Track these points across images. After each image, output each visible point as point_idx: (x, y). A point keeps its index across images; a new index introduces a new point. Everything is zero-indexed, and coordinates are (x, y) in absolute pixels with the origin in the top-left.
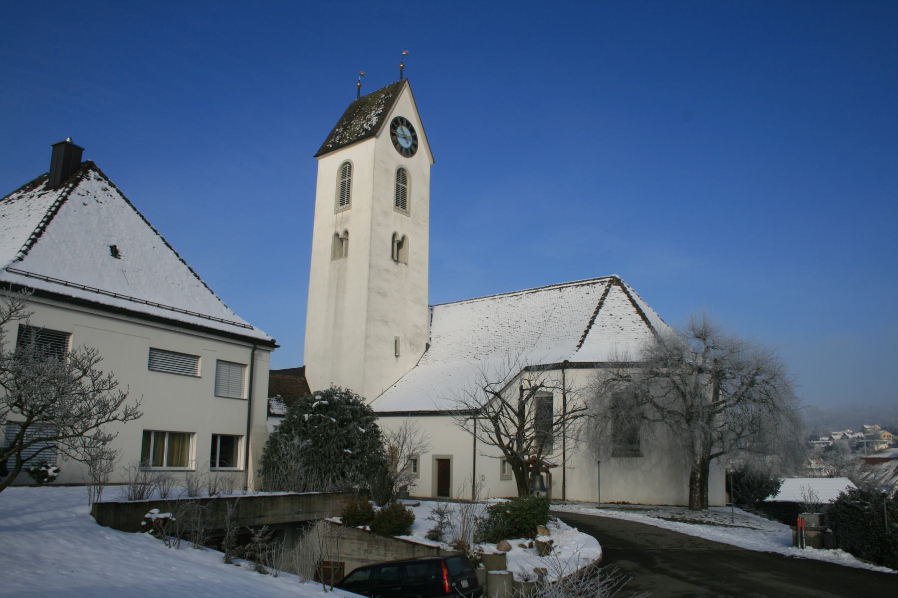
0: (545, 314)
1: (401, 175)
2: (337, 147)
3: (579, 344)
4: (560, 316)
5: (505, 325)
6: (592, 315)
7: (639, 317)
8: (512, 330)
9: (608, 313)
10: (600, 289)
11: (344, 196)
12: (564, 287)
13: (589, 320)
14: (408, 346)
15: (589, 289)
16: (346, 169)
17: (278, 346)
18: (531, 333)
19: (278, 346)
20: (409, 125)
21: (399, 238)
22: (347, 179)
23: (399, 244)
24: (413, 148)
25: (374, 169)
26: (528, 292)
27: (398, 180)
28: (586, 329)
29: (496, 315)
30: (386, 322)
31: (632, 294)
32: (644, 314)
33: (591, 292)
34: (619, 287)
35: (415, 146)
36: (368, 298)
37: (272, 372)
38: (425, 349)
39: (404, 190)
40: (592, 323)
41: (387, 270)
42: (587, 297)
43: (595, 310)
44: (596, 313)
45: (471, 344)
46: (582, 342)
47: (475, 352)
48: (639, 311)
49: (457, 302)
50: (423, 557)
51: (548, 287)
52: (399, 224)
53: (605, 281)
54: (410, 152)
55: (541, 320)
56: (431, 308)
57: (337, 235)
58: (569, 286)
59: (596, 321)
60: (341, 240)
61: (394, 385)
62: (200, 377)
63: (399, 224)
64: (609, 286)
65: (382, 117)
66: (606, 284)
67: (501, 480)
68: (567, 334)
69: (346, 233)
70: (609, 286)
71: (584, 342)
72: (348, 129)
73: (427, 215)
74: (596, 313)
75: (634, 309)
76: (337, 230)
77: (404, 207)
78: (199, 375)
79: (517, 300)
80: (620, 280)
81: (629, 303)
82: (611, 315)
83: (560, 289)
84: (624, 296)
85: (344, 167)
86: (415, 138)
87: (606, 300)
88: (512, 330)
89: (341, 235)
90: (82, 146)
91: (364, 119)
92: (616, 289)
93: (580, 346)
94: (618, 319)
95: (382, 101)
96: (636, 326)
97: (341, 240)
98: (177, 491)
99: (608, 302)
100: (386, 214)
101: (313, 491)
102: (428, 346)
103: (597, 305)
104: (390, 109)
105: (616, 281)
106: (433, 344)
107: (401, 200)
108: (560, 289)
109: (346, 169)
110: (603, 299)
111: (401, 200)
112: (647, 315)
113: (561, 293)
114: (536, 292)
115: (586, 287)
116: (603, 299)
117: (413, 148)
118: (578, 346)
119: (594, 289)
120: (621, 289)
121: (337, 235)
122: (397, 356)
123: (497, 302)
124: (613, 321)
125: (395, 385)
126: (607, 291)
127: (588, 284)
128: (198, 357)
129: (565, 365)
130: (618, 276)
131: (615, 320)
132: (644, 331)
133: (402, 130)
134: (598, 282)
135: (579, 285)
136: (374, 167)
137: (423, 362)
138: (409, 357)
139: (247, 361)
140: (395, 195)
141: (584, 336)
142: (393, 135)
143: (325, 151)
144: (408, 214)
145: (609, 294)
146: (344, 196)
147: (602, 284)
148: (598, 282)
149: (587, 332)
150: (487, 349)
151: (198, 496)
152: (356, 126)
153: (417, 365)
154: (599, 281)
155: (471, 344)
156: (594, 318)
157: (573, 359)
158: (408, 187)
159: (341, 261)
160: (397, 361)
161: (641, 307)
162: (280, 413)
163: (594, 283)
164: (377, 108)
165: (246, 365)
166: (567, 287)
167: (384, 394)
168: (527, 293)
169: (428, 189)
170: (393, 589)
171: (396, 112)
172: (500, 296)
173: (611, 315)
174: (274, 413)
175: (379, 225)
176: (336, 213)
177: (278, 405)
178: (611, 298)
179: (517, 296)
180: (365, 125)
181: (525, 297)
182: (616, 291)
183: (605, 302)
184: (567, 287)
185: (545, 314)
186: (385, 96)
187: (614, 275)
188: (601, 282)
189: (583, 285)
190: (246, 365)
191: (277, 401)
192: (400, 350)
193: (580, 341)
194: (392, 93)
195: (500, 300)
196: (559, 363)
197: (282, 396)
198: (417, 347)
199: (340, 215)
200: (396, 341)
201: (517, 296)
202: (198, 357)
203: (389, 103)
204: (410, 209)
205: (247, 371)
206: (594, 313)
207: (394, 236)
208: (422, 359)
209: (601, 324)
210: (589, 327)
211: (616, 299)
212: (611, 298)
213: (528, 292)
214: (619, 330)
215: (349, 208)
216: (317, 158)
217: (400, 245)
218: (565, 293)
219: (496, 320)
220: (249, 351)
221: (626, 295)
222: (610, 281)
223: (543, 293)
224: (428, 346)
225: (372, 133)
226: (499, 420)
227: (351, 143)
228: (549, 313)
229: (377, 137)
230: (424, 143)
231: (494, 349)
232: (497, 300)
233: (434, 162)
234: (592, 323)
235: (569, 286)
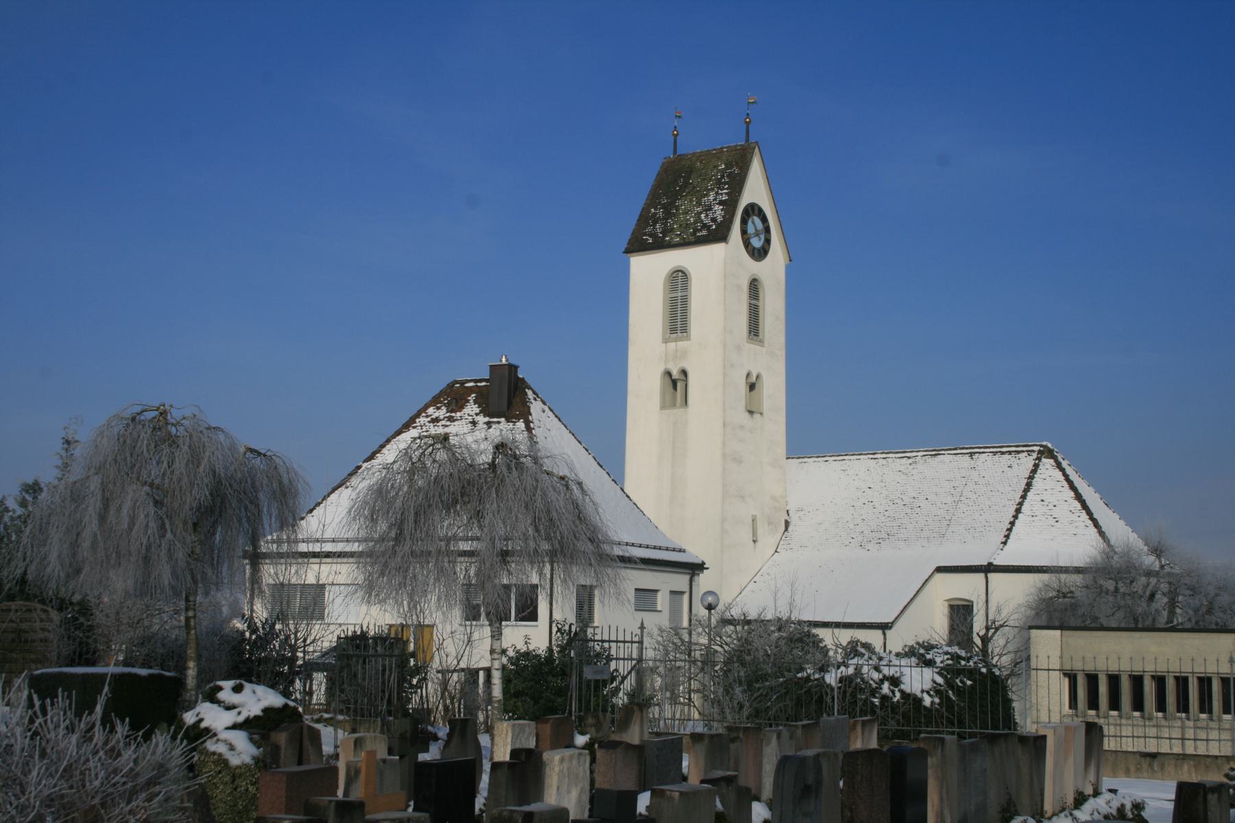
0: (953, 491)
2: (660, 245)
3: (1004, 540)
4: (974, 496)
5: (898, 501)
6: (1018, 500)
7: (1078, 505)
8: (909, 511)
9: (1039, 498)
10: (1027, 462)
12: (977, 453)
13: (1015, 507)
15: (1013, 459)
16: (679, 279)
17: (707, 568)
18: (936, 518)
19: (707, 568)
20: (764, 219)
22: (680, 294)
25: (725, 289)
26: (925, 453)
28: (1012, 520)
29: (883, 484)
30: (743, 497)
31: (1069, 471)
32: (1085, 501)
33: (1015, 466)
34: (1052, 461)
36: (724, 469)
38: (783, 528)
39: (757, 307)
40: (1018, 511)
41: (742, 427)
42: (1009, 472)
43: (1021, 493)
44: (1024, 497)
45: (852, 526)
46: (1007, 537)
47: (860, 539)
48: (1079, 497)
49: (818, 457)
51: (954, 448)
53: (1033, 451)
54: (759, 254)
55: (949, 500)
57: (669, 374)
58: (984, 453)
59: (1024, 508)
61: (753, 580)
62: (661, 611)
64: (1039, 459)
66: (1035, 455)
68: (986, 524)
69: (684, 373)
70: (1039, 459)
71: (1011, 537)
72: (674, 215)
74: (1024, 497)
75: (1072, 494)
76: (668, 367)
77: (757, 335)
78: (659, 608)
79: (910, 464)
80: (1053, 450)
81: (1065, 484)
82: (1042, 501)
83: (971, 454)
84: (1059, 474)
85: (674, 275)
86: (767, 230)
87: (1035, 479)
88: (909, 511)
89: (675, 374)
90: (1123, 706)
91: (699, 204)
92: (1047, 463)
93: (1005, 543)
94: (1051, 507)
95: (723, 177)
96: (1074, 517)
98: (529, 726)
99: (1037, 482)
100: (739, 348)
101: (51, 667)
102: (787, 524)
103: (1023, 486)
104: (739, 195)
105: (1048, 453)
106: (794, 519)
107: (754, 329)
108: (971, 454)
109: (679, 279)
110: (1031, 478)
111: (754, 329)
112: (1089, 503)
113: (972, 462)
114: (936, 455)
115: (1007, 456)
116: (1031, 478)
118: (1002, 543)
119: (1019, 462)
120: (1054, 464)
122: (755, 541)
123: (880, 464)
124: (1045, 509)
125: (754, 580)
126: (1036, 467)
127: (1010, 453)
128: (656, 591)
129: (989, 569)
130: (1049, 445)
131: (1048, 508)
132: (1084, 524)
133: (755, 223)
134: (1023, 451)
135: (997, 452)
136: (725, 286)
137: (785, 546)
138: (768, 540)
139: (686, 589)
141: (1010, 530)
142: (744, 232)
143: (638, 245)
144: (761, 342)
145: (1039, 471)
147: (1029, 455)
148: (1023, 451)
149: (1012, 523)
150: (878, 535)
152: (686, 213)
153: (776, 551)
154: (1024, 449)
155: (852, 526)
156: (1021, 504)
157: (998, 561)
158: (760, 304)
159: (678, 412)
160: (755, 547)
161: (1080, 491)
163: (1018, 452)
164: (719, 188)
165: (682, 593)
166: (980, 453)
167: (743, 593)
168: (924, 456)
171: (744, 201)
172: (884, 456)
173: (1042, 501)
175: (732, 366)
176: (666, 342)
178: (1041, 476)
179: (909, 458)
180: (703, 216)
181: (921, 462)
182: (1048, 466)
183: (1034, 482)
184: (980, 453)
185: (953, 491)
186: (727, 168)
187: (1044, 443)
188: (1027, 451)
189: (1003, 453)
190: (682, 593)
193: (1005, 536)
194: (737, 164)
195: (884, 462)
196: (982, 566)
199: (672, 345)
201: (909, 458)
202: (656, 591)
204: (764, 336)
205: (686, 597)
206: (1021, 498)
207: (748, 375)
208: (782, 542)
209: (1030, 513)
210: (1016, 517)
211: (1048, 478)
212: (1041, 476)
213: (925, 453)
214: (1053, 522)
215: (688, 338)
216: (629, 255)
218: (979, 463)
219: (884, 492)
220: (687, 577)
221: (1061, 473)
222: (1039, 452)
223: (946, 458)
224: (787, 524)
225: (718, 235)
228: (958, 490)
229: (727, 243)
231: (887, 537)
232: (880, 460)
233: (790, 260)
234: (1018, 511)
235: (984, 453)
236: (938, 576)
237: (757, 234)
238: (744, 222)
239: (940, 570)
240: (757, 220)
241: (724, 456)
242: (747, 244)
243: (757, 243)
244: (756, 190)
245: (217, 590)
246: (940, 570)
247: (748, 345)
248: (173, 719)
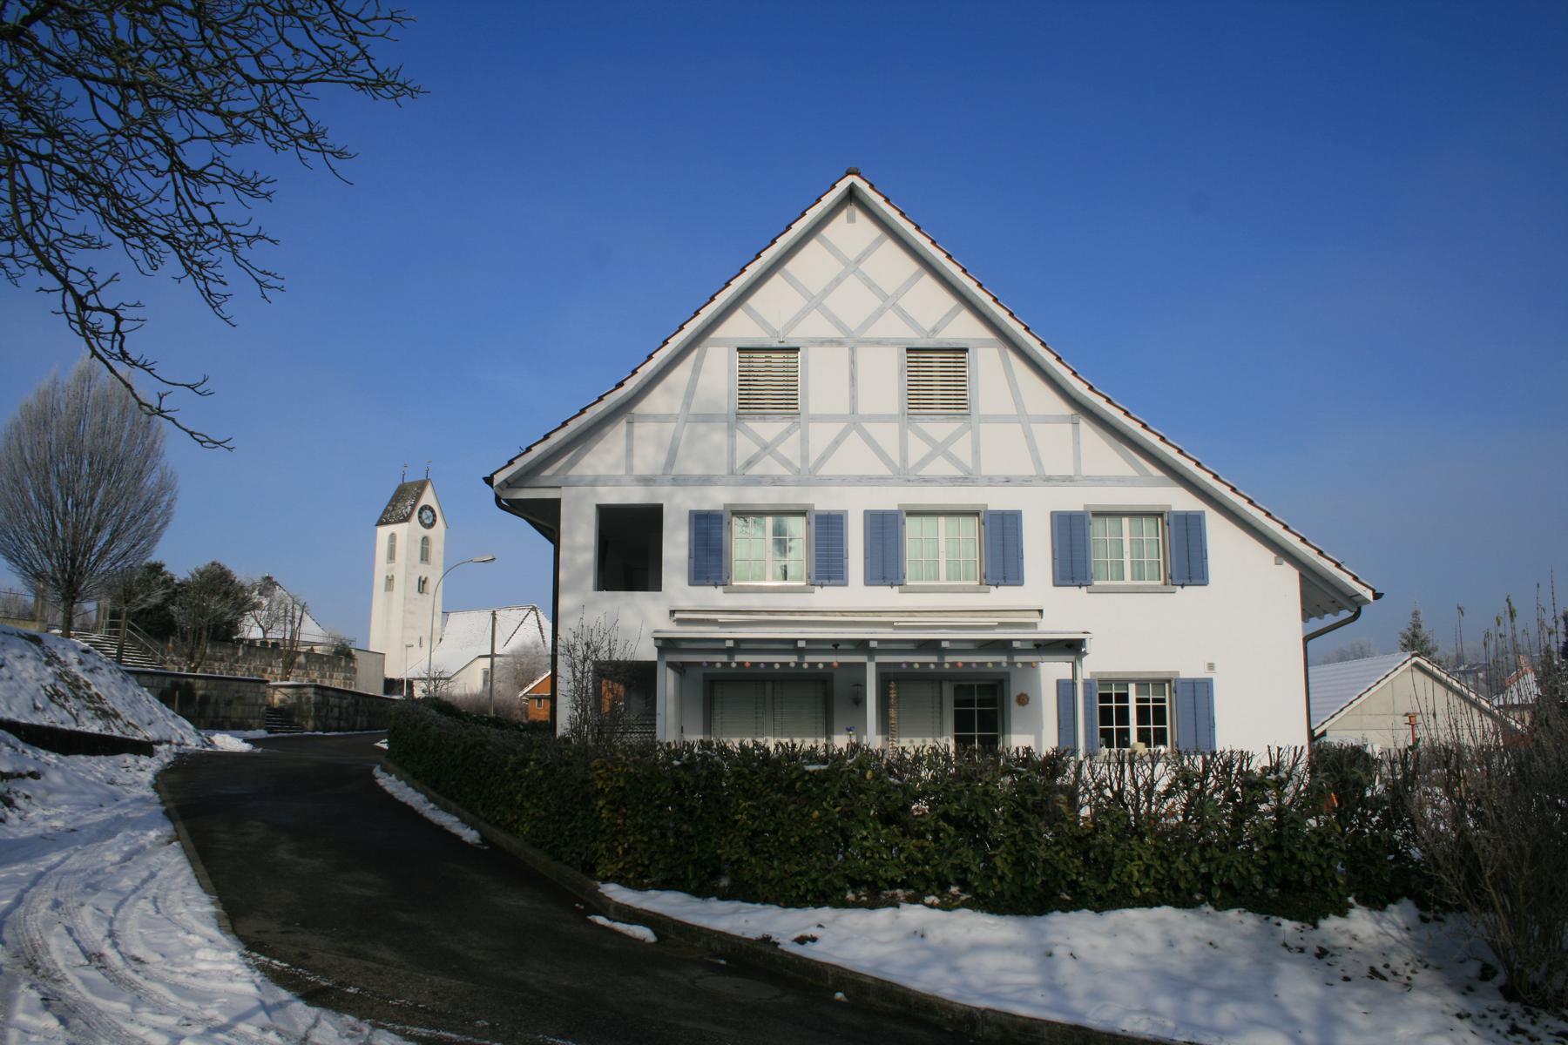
1: (425, 540)
2: (388, 523)
10: (526, 612)
11: (392, 556)
16: (393, 537)
20: (432, 511)
21: (423, 579)
23: (422, 584)
35: (435, 521)
39: (427, 549)
50: (1011, 1001)
52: (423, 571)
54: (431, 526)
56: (446, 613)
60: (390, 581)
63: (423, 571)
65: (413, 507)
67: (1058, 681)
86: (435, 516)
97: (390, 581)
102: (441, 640)
105: (534, 609)
107: (425, 557)
109: (393, 537)
111: (425, 557)
121: (387, 577)
142: (420, 517)
143: (381, 523)
144: (429, 564)
146: (392, 556)
151: (897, 698)
170: (601, 920)
171: (422, 503)
203: (418, 496)
207: (420, 578)
217: (424, 582)
224: (441, 640)
225: (406, 519)
227: (395, 522)
236: (1311, 643)
237: (428, 518)
238: (420, 513)
239: (480, 657)
240: (429, 513)
241: (404, 611)
242: (422, 522)
243: (428, 522)
244: (428, 498)
245: (56, 673)
246: (480, 657)
248: (497, 717)
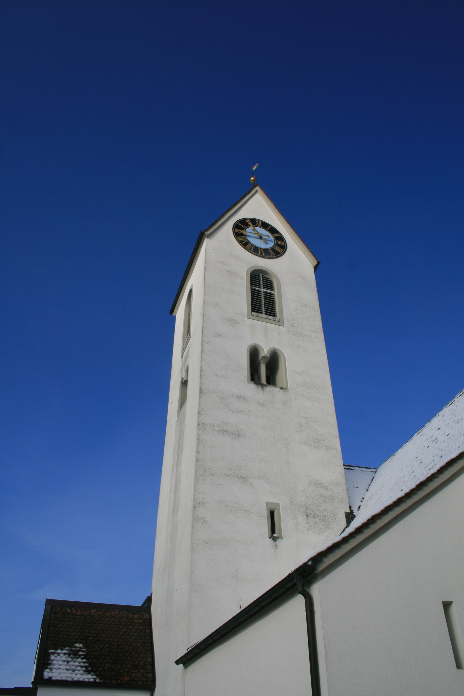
14: (302, 519)
24: (280, 242)
27: (252, 283)
30: (244, 479)
35: (279, 238)
37: (49, 602)
38: (346, 524)
73: (318, 323)
77: (274, 315)
117: (280, 242)
140: (250, 294)
144: (280, 323)
158: (275, 292)
162: (64, 678)
169: (315, 293)
174: (50, 678)
177: (68, 662)
191: (69, 655)
192: (282, 526)
197: (85, 646)
198: (324, 521)
200: (272, 514)
226: (89, 678)
230: (296, 244)
247: (250, 322)
